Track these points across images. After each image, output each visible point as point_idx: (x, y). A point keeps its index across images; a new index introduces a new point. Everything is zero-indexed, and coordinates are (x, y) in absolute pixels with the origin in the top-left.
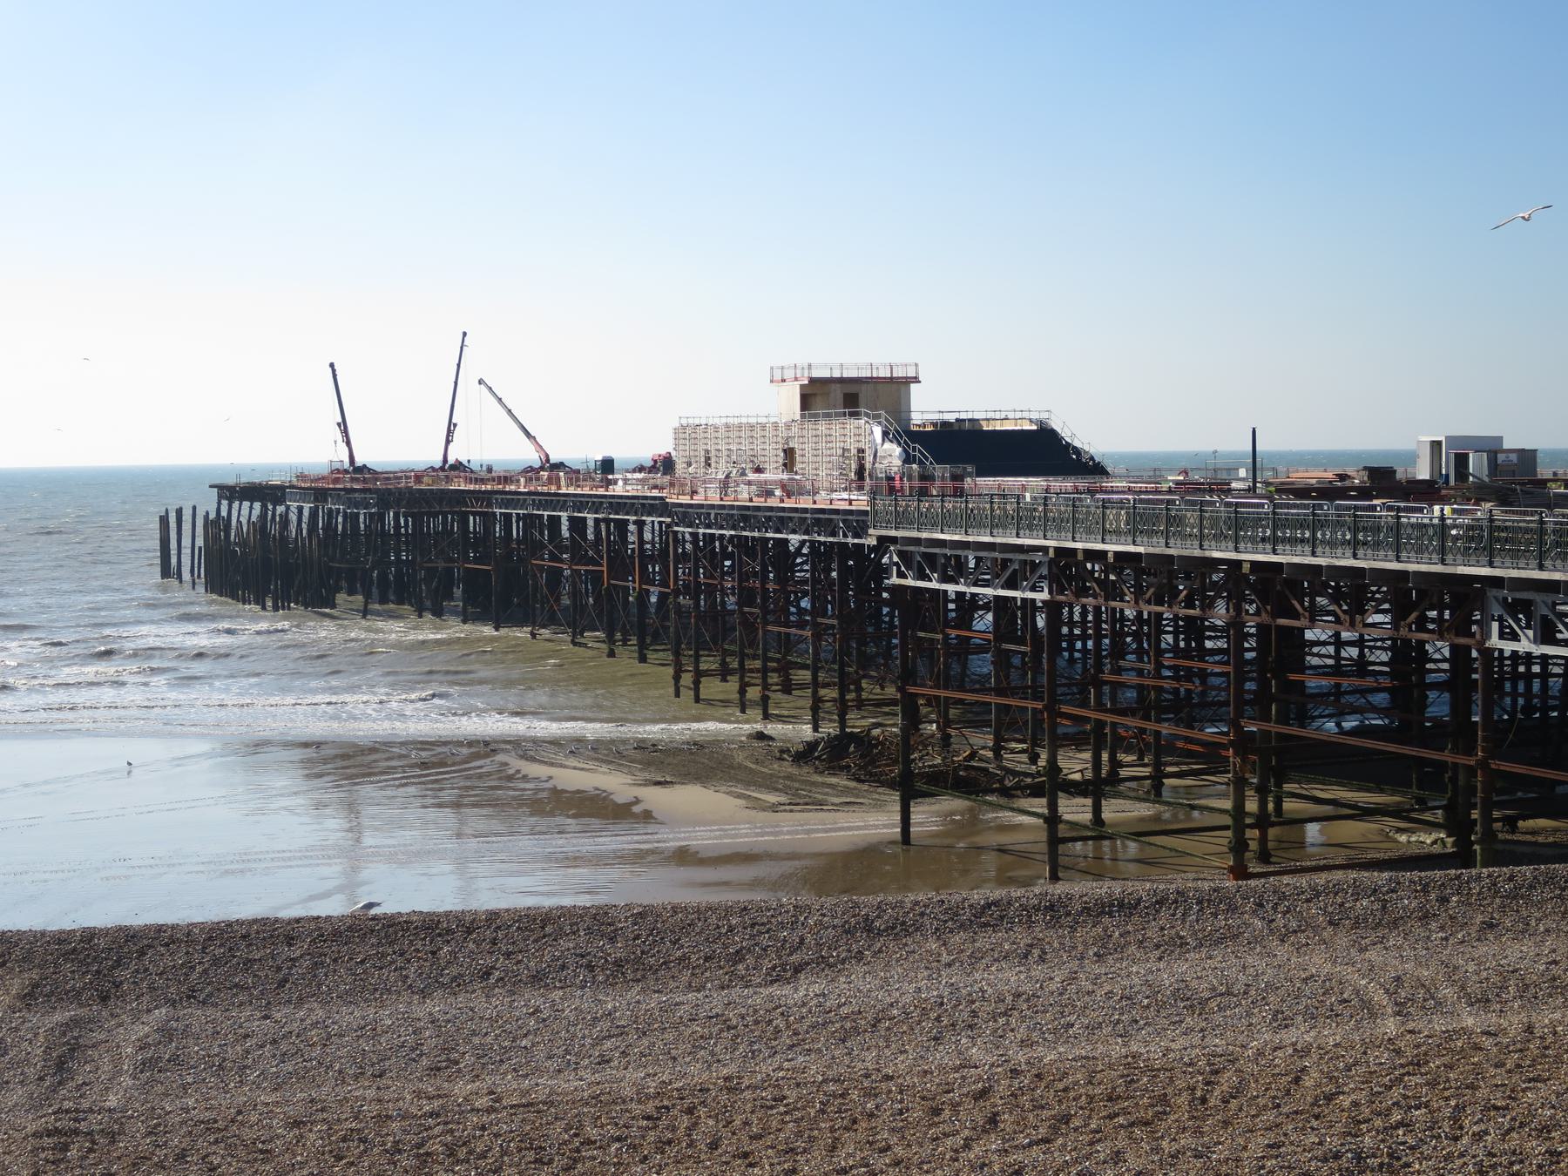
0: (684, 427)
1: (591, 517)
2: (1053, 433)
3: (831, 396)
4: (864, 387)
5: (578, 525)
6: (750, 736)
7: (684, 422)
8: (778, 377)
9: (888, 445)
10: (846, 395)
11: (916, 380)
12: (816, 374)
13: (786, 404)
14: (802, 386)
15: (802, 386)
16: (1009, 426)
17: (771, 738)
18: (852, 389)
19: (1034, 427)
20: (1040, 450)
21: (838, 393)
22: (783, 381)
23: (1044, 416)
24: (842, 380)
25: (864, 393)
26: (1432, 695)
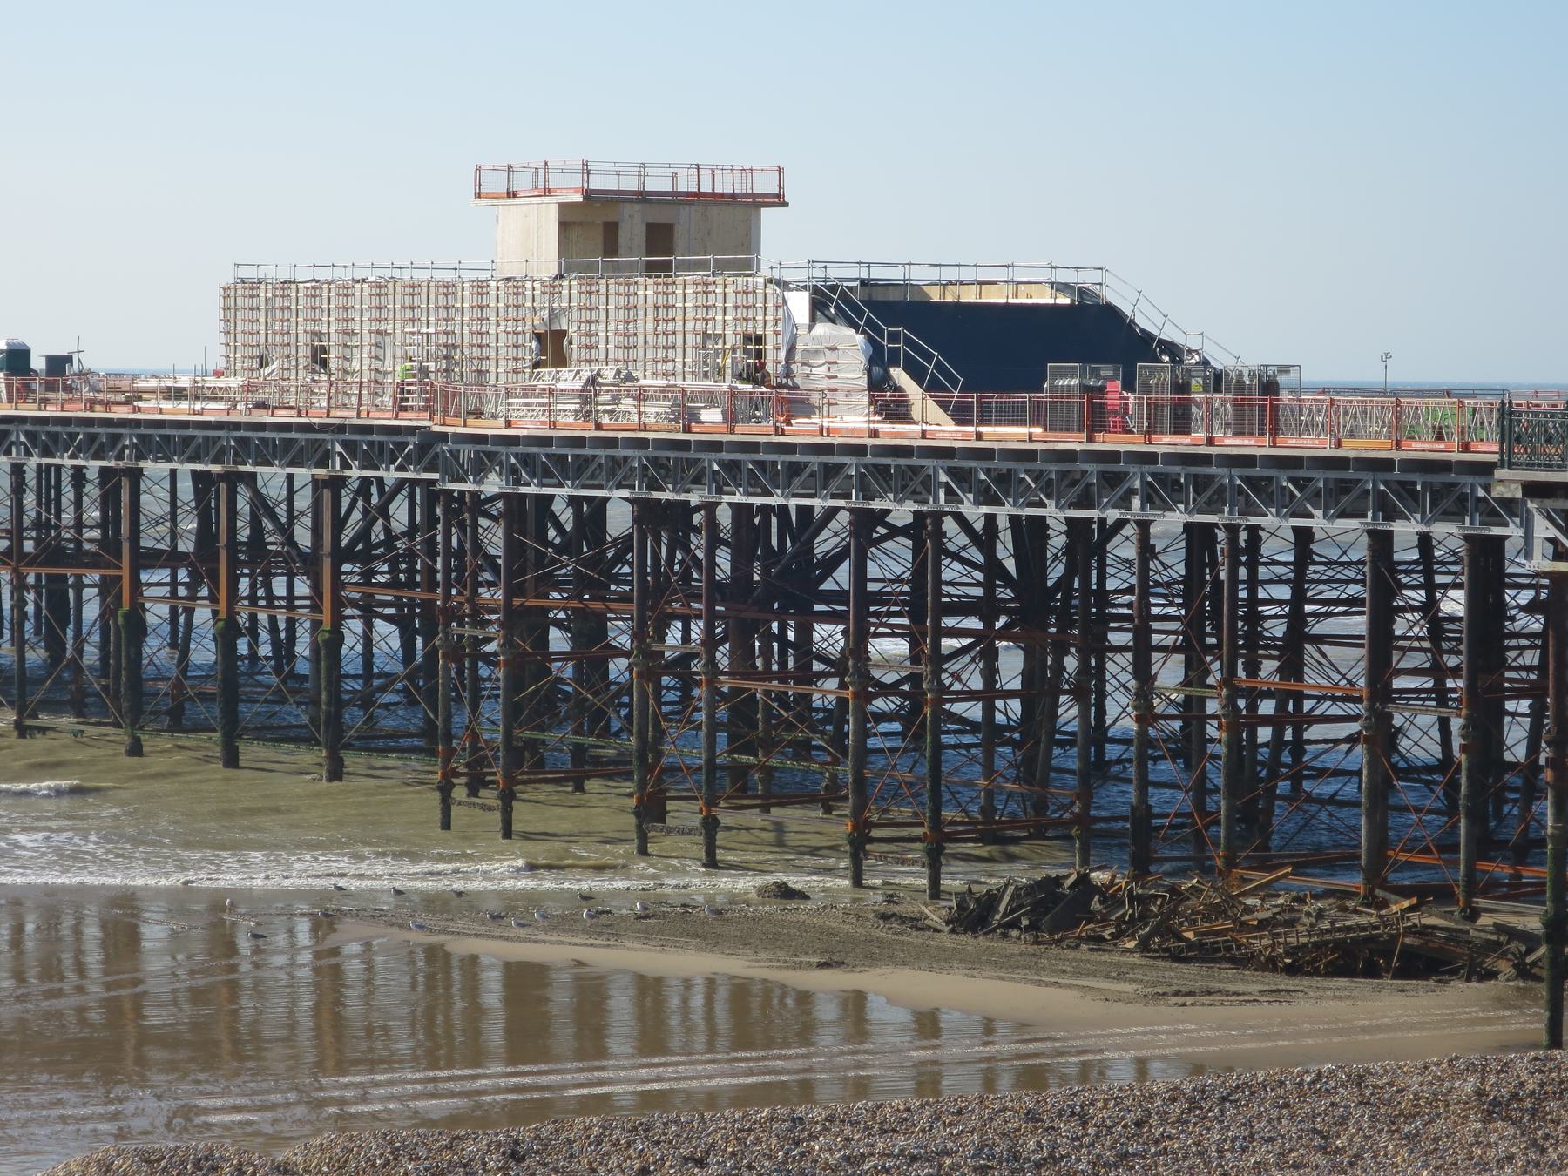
0: (254, 286)
1: (1054, 514)
2: (1111, 311)
3: (633, 231)
4: (684, 211)
5: (592, 516)
6: (762, 891)
7: (249, 274)
8: (495, 182)
9: (822, 328)
10: (651, 228)
11: (778, 200)
12: (598, 183)
13: (527, 241)
14: (564, 208)
15: (564, 208)
16: (969, 296)
17: (803, 896)
18: (661, 216)
19: (1064, 300)
20: (1092, 331)
21: (633, 229)
22: (512, 194)
23: (1087, 279)
24: (643, 197)
25: (686, 223)
26: (1016, 685)
